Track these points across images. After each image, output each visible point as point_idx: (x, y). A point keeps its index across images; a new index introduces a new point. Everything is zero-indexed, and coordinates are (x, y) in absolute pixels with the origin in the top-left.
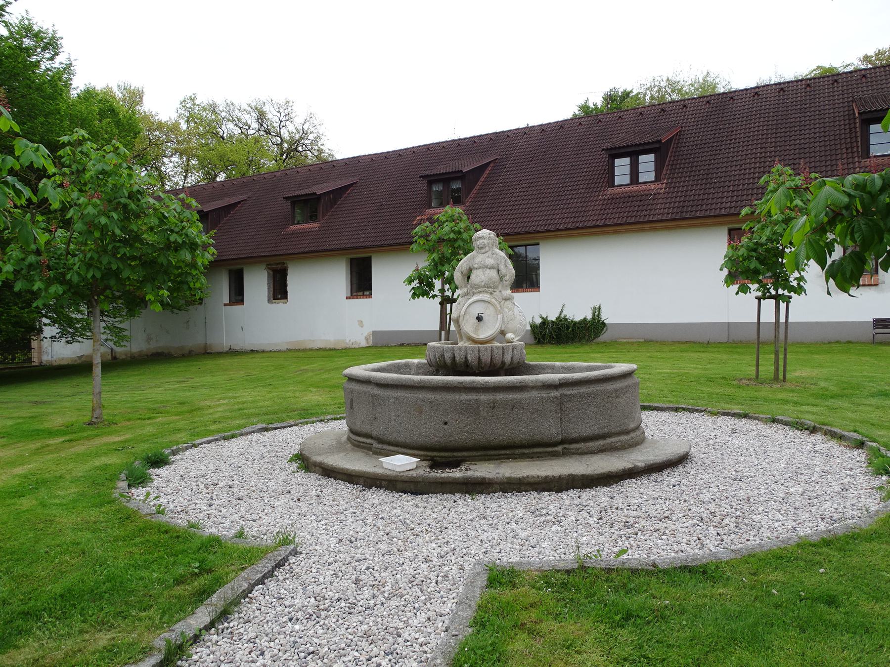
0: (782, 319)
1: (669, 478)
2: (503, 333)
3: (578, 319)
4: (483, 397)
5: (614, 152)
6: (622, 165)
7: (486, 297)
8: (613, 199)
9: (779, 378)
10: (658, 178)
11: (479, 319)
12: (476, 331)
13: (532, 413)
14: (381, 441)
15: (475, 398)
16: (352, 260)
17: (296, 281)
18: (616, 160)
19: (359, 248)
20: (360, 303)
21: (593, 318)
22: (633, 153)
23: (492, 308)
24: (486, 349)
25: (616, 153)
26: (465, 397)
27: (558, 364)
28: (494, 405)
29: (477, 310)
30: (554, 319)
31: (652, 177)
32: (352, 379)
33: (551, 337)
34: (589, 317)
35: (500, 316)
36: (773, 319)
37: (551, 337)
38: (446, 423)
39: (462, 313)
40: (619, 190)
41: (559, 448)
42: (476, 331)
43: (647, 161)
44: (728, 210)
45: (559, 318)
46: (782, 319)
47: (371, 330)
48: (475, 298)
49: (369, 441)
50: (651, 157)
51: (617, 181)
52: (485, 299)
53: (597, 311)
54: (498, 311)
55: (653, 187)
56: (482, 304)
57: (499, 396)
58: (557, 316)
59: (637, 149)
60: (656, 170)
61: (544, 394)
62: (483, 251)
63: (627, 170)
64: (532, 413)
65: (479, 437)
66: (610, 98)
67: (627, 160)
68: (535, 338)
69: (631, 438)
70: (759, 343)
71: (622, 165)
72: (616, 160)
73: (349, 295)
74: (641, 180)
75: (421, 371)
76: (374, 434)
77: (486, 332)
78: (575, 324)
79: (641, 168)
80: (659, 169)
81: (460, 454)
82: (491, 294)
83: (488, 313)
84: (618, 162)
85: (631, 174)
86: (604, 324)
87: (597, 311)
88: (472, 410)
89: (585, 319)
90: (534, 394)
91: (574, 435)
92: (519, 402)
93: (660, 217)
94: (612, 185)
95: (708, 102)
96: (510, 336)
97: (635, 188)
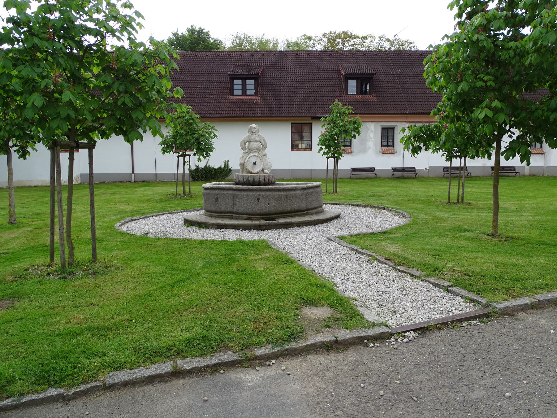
1: (335, 222)
2: (263, 170)
3: (216, 167)
4: (283, 193)
5: (234, 77)
6: (237, 84)
7: (256, 154)
8: (234, 102)
9: (335, 191)
10: (256, 94)
11: (255, 163)
12: (253, 169)
18: (235, 81)
21: (225, 167)
22: (244, 78)
23: (259, 159)
24: (257, 176)
25: (234, 77)
26: (276, 193)
27: (284, 183)
28: (287, 196)
29: (253, 160)
30: (203, 167)
31: (253, 92)
32: (206, 189)
33: (202, 177)
34: (223, 166)
37: (202, 177)
39: (246, 161)
40: (236, 98)
41: (305, 212)
42: (253, 169)
43: (251, 84)
45: (205, 167)
47: (79, 174)
48: (250, 156)
50: (253, 82)
51: (235, 93)
53: (227, 163)
54: (261, 160)
55: (254, 98)
57: (288, 193)
58: (205, 165)
59: (246, 76)
61: (302, 192)
63: (240, 87)
65: (281, 209)
66: (191, 31)
67: (240, 82)
68: (193, 178)
69: (318, 209)
71: (237, 84)
72: (235, 81)
74: (247, 94)
77: (257, 169)
78: (215, 170)
79: (248, 87)
80: (256, 89)
83: (258, 161)
85: (242, 90)
86: (230, 170)
87: (227, 163)
88: (279, 198)
89: (220, 167)
90: (299, 192)
91: (310, 207)
93: (260, 115)
94: (232, 94)
95: (274, 55)
96: (266, 171)
97: (245, 97)
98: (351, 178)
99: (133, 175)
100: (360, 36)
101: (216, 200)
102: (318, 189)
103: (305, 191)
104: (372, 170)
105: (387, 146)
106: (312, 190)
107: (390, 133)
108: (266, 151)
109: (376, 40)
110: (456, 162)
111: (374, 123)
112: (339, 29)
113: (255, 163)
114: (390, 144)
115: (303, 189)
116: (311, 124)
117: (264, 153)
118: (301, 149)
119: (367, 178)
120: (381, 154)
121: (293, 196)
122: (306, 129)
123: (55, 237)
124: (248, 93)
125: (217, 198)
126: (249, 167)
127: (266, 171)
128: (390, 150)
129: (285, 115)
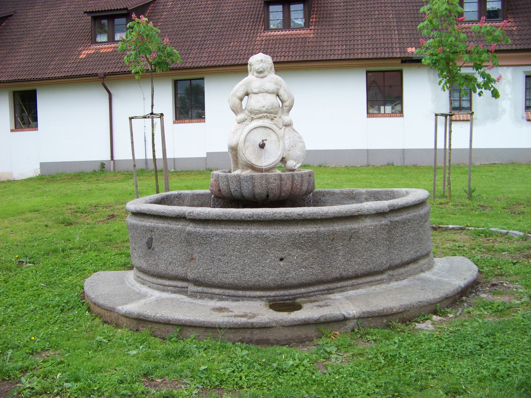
0: (447, 147)
2: (283, 160)
7: (266, 122)
10: (307, 25)
11: (262, 146)
13: (367, 243)
14: (197, 282)
15: (315, 230)
16: (15, 93)
17: (48, 106)
19: (22, 81)
20: (26, 135)
23: (273, 134)
29: (258, 137)
35: (281, 143)
36: (443, 147)
38: (281, 259)
41: (385, 276)
44: (340, 56)
46: (447, 147)
49: (185, 284)
52: (267, 125)
56: (263, 130)
60: (305, 17)
62: (261, 75)
63: (280, 16)
64: (367, 243)
67: (279, 8)
70: (156, 171)
73: (14, 128)
74: (272, 27)
75: (195, 203)
76: (190, 276)
77: (269, 159)
79: (293, 16)
80: (307, 17)
81: (293, 292)
82: (272, 119)
84: (272, 8)
90: (368, 223)
92: (334, 233)
94: (267, 28)
96: (291, 163)
99: (112, 162)
102: (422, 211)
103: (384, 221)
106: (405, 216)
108: (293, 116)
111: (511, 69)
113: (262, 146)
115: (380, 214)
116: (401, 72)
117: (286, 119)
120: (525, 121)
121: (352, 235)
125: (151, 239)
126: (249, 154)
127: (291, 163)
129: (356, 57)
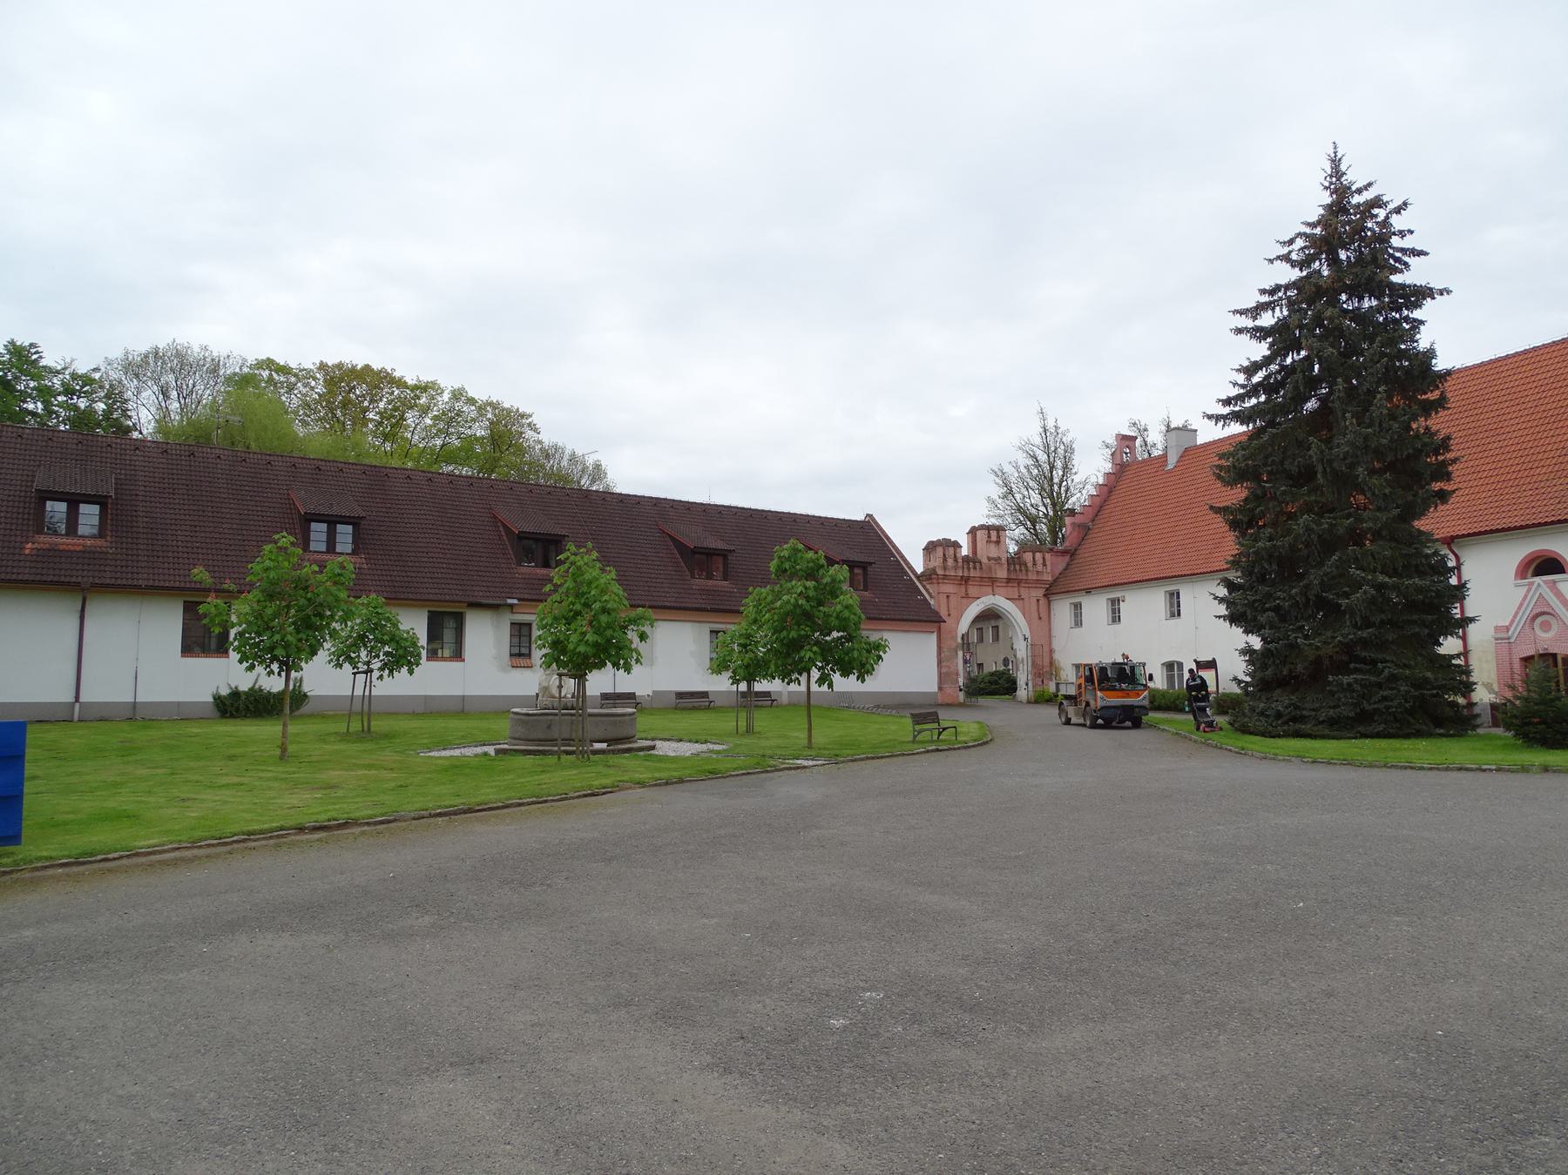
6: (57, 509)
31: (349, 548)
45: (252, 689)
63: (324, 537)
67: (324, 527)
71: (319, 530)
86: (305, 695)
98: (676, 708)
100: (410, 380)
101: (549, 727)
104: (704, 694)
105: (520, 655)
107: (525, 631)
109: (446, 396)
110: (743, 687)
112: (357, 355)
114: (524, 651)
118: (443, 659)
119: (694, 708)
122: (450, 624)
123: (674, 745)
124: (82, 530)
128: (522, 661)
